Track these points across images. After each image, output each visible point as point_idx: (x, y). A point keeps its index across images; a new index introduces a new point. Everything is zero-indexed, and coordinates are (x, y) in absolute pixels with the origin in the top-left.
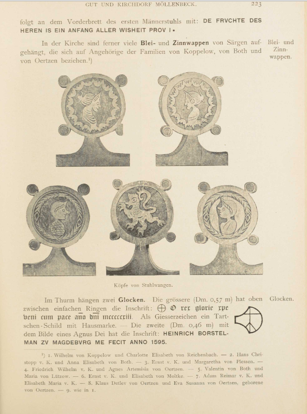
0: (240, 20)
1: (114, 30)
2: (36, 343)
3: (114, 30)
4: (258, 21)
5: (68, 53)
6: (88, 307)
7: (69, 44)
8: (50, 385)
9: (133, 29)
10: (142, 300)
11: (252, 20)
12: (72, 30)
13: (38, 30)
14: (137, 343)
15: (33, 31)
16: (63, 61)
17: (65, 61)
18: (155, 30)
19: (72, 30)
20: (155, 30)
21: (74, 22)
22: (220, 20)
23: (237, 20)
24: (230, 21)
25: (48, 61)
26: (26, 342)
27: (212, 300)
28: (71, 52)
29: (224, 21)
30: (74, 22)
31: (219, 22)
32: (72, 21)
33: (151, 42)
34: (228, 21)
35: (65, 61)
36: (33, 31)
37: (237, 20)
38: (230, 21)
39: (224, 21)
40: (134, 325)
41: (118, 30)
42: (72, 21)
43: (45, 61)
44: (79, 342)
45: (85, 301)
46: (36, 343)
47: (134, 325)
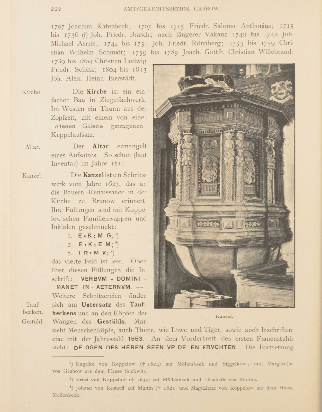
2: (101, 348)
4: (114, 348)
6: (194, 42)
7: (56, 202)
8: (140, 390)
9: (123, 346)
11: (108, 347)
12: (65, 287)
13: (159, 347)
15: (135, 347)
16: (24, 312)
17: (26, 312)
18: (208, 346)
19: (65, 287)
20: (208, 346)
21: (188, 339)
22: (206, 347)
23: (224, 347)
24: (217, 347)
27: (87, 347)
28: (61, 305)
30: (188, 339)
31: (205, 349)
32: (186, 338)
34: (214, 347)
35: (26, 312)
36: (135, 347)
37: (224, 347)
42: (210, 33)
44: (98, 278)
45: (182, 35)
46: (101, 348)
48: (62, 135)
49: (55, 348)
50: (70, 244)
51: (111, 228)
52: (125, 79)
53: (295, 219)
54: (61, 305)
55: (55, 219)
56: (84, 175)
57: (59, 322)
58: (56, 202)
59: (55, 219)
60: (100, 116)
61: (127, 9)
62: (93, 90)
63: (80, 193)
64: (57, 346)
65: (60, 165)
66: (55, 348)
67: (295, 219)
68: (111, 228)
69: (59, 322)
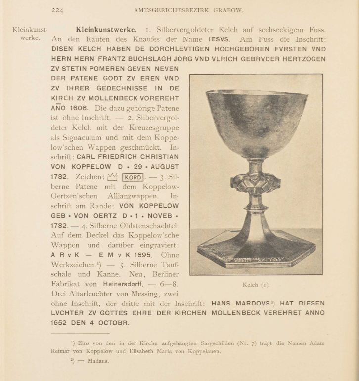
0: (74, 313)
1: (169, 313)
3: (169, 313)
5: (81, 265)
7: (144, 344)
10: (23, 38)
11: (159, 313)
12: (112, 59)
14: (313, 314)
23: (70, 313)
24: (62, 313)
25: (66, 197)
26: (323, 303)
28: (89, 128)
29: (261, 59)
33: (88, 28)
34: (55, 167)
37: (70, 313)
38: (62, 313)
39: (261, 59)
40: (98, 108)
41: (173, 313)
43: (63, 197)
47: (98, 108)
48: (167, 138)
49: (56, 323)
50: (53, 255)
51: (157, 148)
52: (150, 352)
53: (168, 10)
54: (89, 128)
55: (155, 236)
56: (77, 30)
57: (59, 246)
58: (144, 344)
59: (155, 236)
60: (146, 244)
61: (138, 10)
62: (168, 273)
63: (61, 187)
64: (171, 224)
65: (179, 31)
66: (56, 323)
67: (168, 10)
68: (157, 148)
69: (59, 246)
